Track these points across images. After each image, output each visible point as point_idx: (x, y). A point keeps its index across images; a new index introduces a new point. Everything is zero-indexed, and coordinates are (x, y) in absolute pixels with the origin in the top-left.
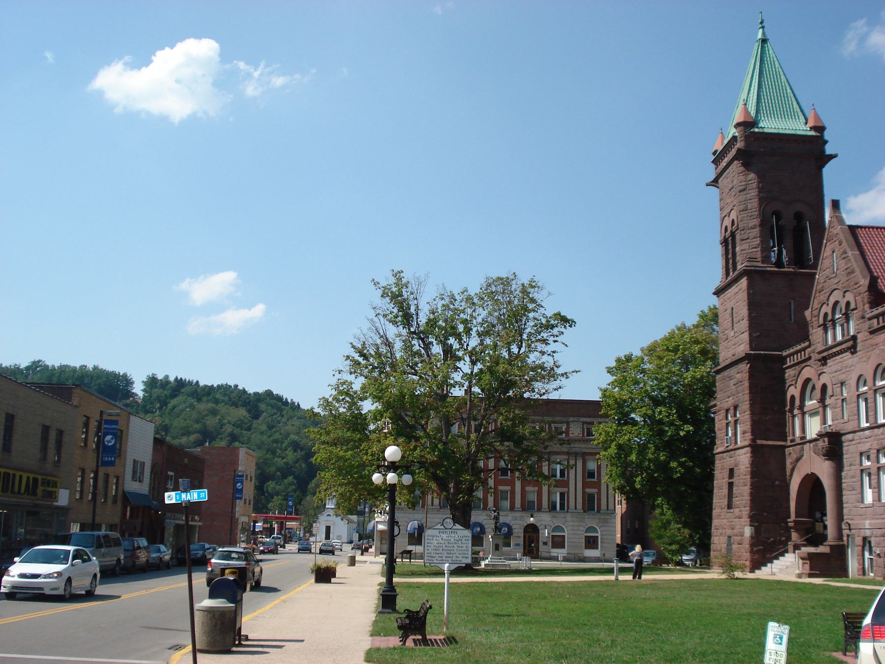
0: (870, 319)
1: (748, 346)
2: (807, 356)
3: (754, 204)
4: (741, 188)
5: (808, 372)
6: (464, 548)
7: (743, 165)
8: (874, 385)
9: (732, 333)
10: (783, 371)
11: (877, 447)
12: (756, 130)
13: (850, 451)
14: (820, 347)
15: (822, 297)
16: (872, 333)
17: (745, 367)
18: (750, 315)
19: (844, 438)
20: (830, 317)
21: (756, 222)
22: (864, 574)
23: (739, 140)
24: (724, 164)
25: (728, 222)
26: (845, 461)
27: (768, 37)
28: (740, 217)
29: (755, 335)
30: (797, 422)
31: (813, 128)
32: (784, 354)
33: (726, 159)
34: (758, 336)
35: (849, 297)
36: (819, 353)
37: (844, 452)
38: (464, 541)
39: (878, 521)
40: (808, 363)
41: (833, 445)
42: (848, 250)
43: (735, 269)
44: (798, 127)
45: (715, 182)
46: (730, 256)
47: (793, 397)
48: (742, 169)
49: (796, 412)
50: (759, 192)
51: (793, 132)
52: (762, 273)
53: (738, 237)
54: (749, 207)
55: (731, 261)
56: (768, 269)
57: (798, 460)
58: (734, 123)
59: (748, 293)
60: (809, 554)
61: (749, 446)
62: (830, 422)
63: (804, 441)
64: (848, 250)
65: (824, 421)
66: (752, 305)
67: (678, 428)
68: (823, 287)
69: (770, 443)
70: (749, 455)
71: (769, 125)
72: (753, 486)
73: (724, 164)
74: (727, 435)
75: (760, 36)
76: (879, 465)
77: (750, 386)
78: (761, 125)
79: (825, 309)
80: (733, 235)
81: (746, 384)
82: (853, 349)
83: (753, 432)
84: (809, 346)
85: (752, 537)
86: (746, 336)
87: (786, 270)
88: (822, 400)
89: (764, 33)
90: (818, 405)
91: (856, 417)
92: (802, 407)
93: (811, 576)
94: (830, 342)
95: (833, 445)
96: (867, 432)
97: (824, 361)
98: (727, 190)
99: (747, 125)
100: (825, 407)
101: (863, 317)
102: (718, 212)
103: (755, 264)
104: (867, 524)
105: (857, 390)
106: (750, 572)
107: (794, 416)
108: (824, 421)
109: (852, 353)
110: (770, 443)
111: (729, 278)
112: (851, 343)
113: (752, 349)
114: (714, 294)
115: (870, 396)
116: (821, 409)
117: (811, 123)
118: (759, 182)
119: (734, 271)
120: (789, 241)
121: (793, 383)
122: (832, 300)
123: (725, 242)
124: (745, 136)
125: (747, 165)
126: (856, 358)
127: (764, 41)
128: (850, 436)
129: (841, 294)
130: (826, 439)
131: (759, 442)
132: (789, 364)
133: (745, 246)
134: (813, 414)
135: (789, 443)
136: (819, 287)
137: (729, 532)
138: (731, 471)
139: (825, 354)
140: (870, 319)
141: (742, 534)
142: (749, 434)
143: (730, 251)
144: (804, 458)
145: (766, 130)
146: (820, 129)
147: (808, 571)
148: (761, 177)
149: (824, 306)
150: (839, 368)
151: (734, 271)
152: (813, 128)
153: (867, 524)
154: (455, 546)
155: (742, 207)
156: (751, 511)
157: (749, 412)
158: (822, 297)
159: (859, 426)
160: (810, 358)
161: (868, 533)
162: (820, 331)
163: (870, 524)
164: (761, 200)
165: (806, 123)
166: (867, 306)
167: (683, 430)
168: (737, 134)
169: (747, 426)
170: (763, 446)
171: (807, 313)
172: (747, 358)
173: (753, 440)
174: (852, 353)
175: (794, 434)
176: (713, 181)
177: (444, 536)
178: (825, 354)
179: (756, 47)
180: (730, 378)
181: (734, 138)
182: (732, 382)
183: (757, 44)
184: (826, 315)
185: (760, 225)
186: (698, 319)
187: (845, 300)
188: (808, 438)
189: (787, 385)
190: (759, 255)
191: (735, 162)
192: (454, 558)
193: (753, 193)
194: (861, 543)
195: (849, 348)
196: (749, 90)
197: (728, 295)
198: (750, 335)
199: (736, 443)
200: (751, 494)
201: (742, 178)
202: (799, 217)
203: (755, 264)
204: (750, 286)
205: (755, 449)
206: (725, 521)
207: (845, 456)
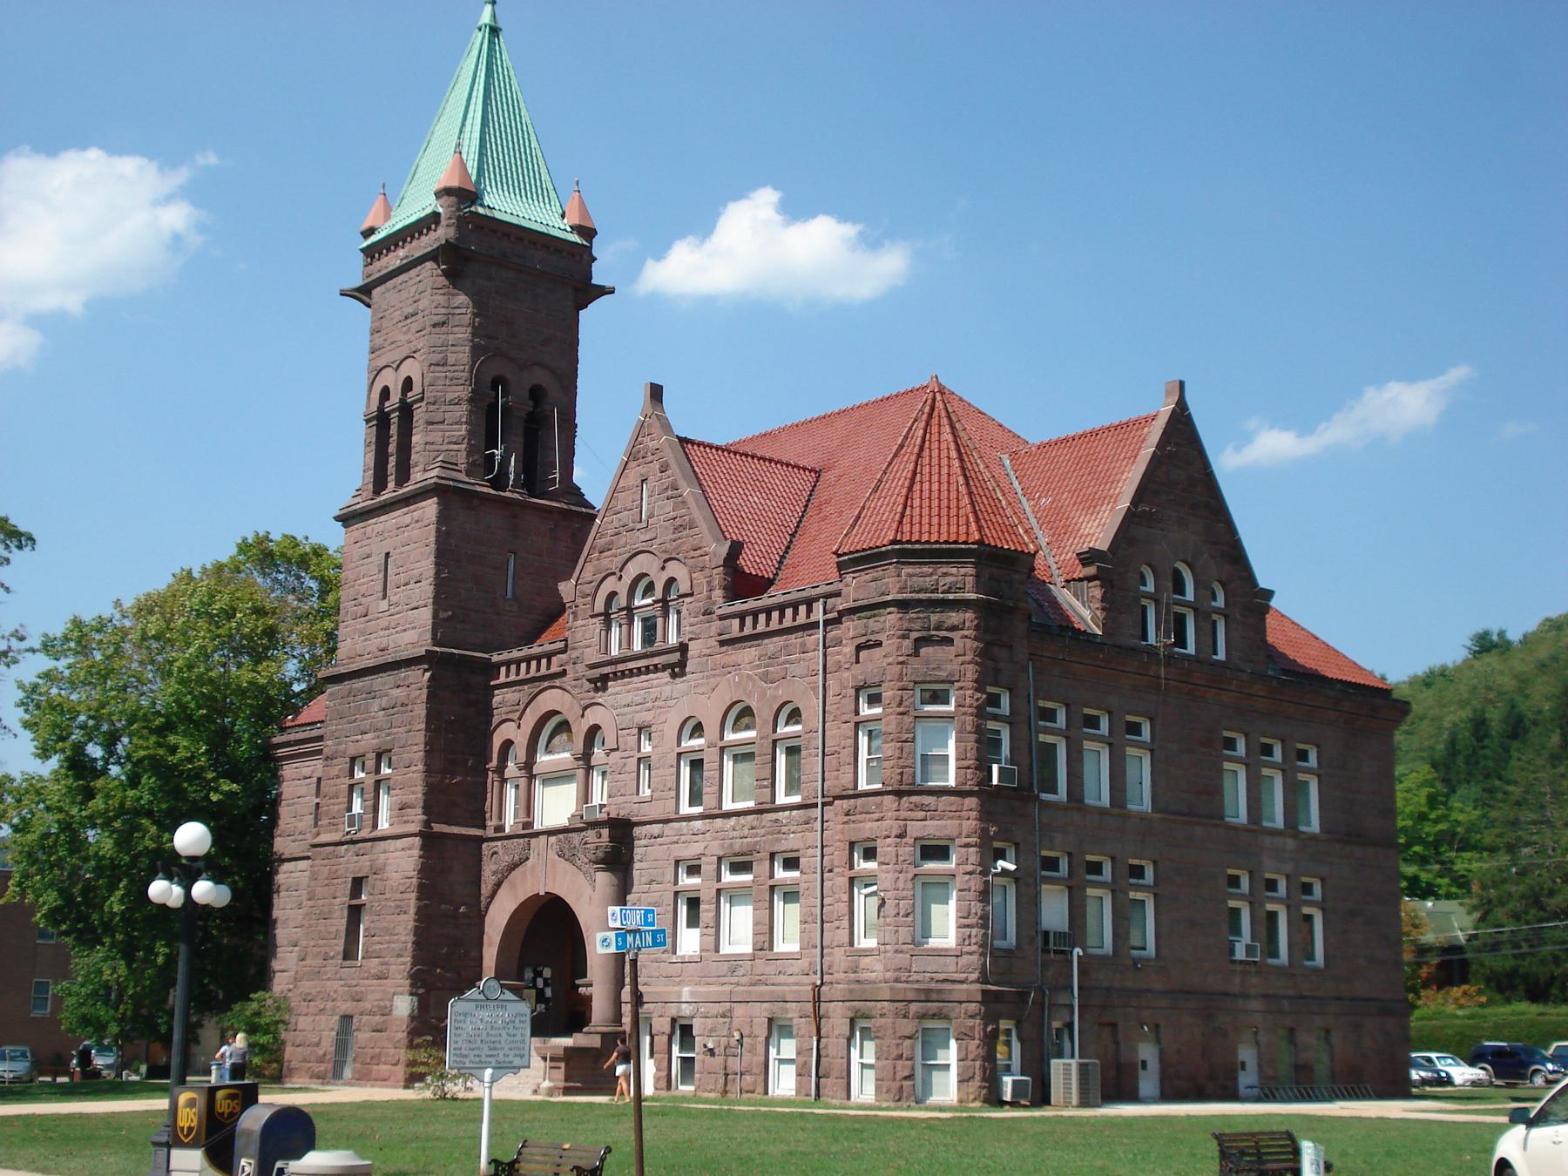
0: (722, 618)
1: (429, 636)
2: (554, 669)
3: (463, 355)
4: (436, 319)
5: (550, 699)
6: (518, 1038)
7: (446, 274)
8: (722, 738)
9: (384, 605)
10: (489, 692)
11: (721, 853)
12: (481, 210)
13: (649, 856)
14: (593, 656)
15: (610, 562)
16: (722, 643)
17: (420, 677)
18: (437, 574)
19: (637, 831)
20: (622, 600)
21: (464, 392)
22: (669, 1087)
23: (443, 222)
24: (394, 260)
25: (392, 380)
26: (636, 873)
27: (500, 25)
28: (429, 377)
29: (443, 615)
30: (510, 793)
31: (579, 229)
32: (495, 658)
33: (401, 253)
34: (446, 620)
35: (674, 569)
36: (592, 667)
37: (636, 857)
38: (517, 1024)
39: (711, 988)
40: (557, 682)
41: (616, 846)
42: (682, 483)
43: (403, 476)
44: (545, 216)
45: (363, 293)
46: (392, 448)
47: (508, 744)
48: (443, 281)
49: (511, 769)
50: (474, 334)
51: (514, 221)
52: (468, 495)
53: (419, 415)
54: (451, 360)
55: (392, 461)
56: (478, 489)
57: (514, 866)
58: (436, 186)
59: (438, 531)
60: (566, 1049)
61: (420, 834)
62: (597, 800)
63: (528, 832)
64: (682, 483)
65: (585, 795)
66: (444, 555)
67: (209, 787)
68: (612, 543)
69: (456, 830)
70: (416, 852)
71: (502, 204)
72: (423, 915)
73: (394, 260)
74: (350, 809)
75: (486, 17)
76: (719, 886)
77: (428, 716)
78: (487, 201)
79: (609, 585)
80: (406, 410)
81: (421, 710)
82: (678, 669)
83: (428, 808)
84: (564, 651)
85: (412, 1018)
86: (425, 615)
87: (508, 494)
88: (586, 757)
89: (494, 16)
90: (572, 764)
91: (673, 793)
92: (528, 765)
93: (567, 1091)
94: (615, 652)
95: (616, 846)
96: (698, 824)
97: (601, 683)
98: (398, 315)
99: (463, 196)
100: (589, 769)
101: (708, 613)
102: (366, 355)
103: (455, 475)
104: (686, 992)
105: (679, 744)
106: (406, 1087)
107: (503, 781)
108: (585, 795)
109: (674, 676)
110: (456, 830)
111: (386, 496)
112: (676, 657)
113: (436, 642)
114: (337, 519)
115: (710, 757)
116: (580, 773)
117: (574, 218)
118: (475, 315)
119: (400, 483)
120: (518, 441)
121: (515, 716)
122: (632, 570)
123: (380, 420)
124: (459, 219)
125: (454, 276)
126: (681, 685)
127: (494, 31)
128: (656, 829)
129: (658, 563)
130: (605, 832)
131: (437, 827)
132: (502, 679)
133: (436, 437)
134: (557, 777)
135: (490, 833)
136: (601, 542)
137: (346, 1007)
138: (358, 884)
139: (606, 670)
140: (722, 618)
141: (386, 1012)
142: (420, 811)
143: (394, 441)
144: (529, 863)
145: (498, 215)
146: (588, 232)
147: (562, 1084)
148: (481, 307)
149: (612, 579)
150: (638, 699)
151: (400, 483)
152: (579, 229)
153: (686, 992)
154: (504, 1033)
155: (436, 358)
156: (414, 965)
157: (421, 767)
158: (610, 562)
159: (677, 812)
160: (564, 673)
161: (686, 1010)
162: (597, 625)
163: (692, 993)
164: (476, 351)
165: (563, 216)
166: (718, 594)
167: (216, 790)
168: (440, 210)
169: (416, 795)
170: (443, 835)
171: (566, 589)
172: (428, 659)
173: (427, 824)
174: (674, 676)
175: (500, 816)
176: (358, 290)
177: (485, 1014)
178: (606, 670)
179: (479, 39)
180: (371, 694)
181: (435, 217)
182: (375, 705)
183: (480, 35)
184: (613, 595)
185: (471, 401)
186: (235, 551)
187: (665, 576)
188: (537, 827)
189: (495, 721)
190: (462, 458)
191: (429, 265)
192: (501, 1058)
193: (463, 334)
194: (667, 1029)
195: (671, 666)
196: (463, 125)
197: (380, 527)
198: (435, 616)
199: (375, 826)
200: (417, 931)
201: (441, 299)
202: (536, 393)
203: (455, 475)
204: (442, 518)
205: (430, 841)
206: (336, 984)
207: (636, 866)
